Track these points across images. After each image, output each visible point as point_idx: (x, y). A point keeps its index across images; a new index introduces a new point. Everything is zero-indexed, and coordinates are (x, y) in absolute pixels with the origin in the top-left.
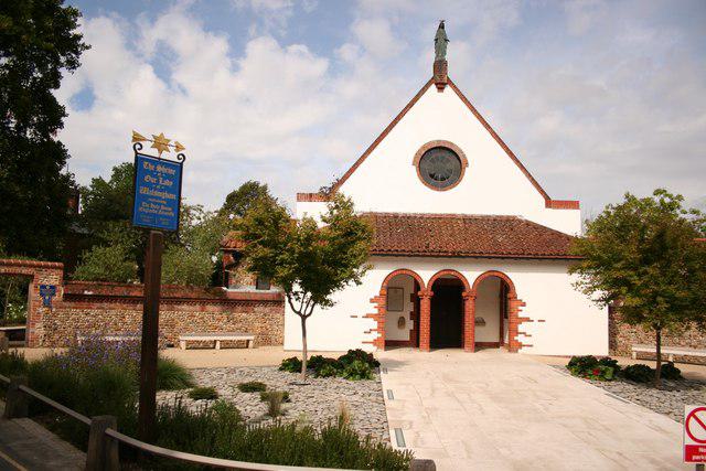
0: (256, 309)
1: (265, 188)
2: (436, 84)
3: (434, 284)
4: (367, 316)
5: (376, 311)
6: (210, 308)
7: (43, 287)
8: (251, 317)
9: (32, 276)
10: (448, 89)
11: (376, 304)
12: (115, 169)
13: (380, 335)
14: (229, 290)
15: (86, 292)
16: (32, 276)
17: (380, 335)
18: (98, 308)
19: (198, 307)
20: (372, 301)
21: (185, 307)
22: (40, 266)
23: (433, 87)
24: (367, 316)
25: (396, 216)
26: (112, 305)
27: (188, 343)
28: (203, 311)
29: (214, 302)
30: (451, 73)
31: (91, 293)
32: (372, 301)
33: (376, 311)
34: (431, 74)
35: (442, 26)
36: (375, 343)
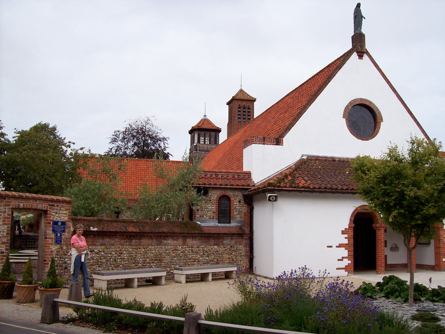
0: (225, 242)
1: (54, 129)
2: (357, 52)
3: (355, 218)
4: (340, 246)
5: (346, 241)
6: (190, 241)
7: (56, 223)
8: (221, 249)
9: (45, 212)
10: (365, 57)
11: (346, 236)
12: (254, 100)
13: (350, 262)
14: (203, 224)
15: (92, 229)
16: (45, 212)
17: (350, 262)
18: (102, 245)
19: (180, 241)
20: (343, 233)
21: (170, 241)
22: (52, 201)
23: (355, 55)
24: (340, 246)
25: (333, 160)
26: (113, 242)
27: (188, 277)
28: (184, 244)
29: (193, 236)
30: (368, 46)
31: (96, 229)
32: (343, 233)
33: (346, 241)
34: (349, 46)
35: (359, 5)
36: (346, 268)
